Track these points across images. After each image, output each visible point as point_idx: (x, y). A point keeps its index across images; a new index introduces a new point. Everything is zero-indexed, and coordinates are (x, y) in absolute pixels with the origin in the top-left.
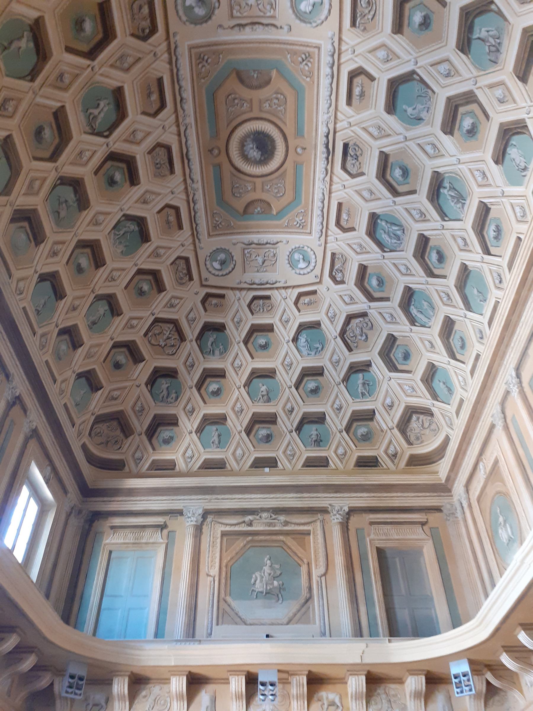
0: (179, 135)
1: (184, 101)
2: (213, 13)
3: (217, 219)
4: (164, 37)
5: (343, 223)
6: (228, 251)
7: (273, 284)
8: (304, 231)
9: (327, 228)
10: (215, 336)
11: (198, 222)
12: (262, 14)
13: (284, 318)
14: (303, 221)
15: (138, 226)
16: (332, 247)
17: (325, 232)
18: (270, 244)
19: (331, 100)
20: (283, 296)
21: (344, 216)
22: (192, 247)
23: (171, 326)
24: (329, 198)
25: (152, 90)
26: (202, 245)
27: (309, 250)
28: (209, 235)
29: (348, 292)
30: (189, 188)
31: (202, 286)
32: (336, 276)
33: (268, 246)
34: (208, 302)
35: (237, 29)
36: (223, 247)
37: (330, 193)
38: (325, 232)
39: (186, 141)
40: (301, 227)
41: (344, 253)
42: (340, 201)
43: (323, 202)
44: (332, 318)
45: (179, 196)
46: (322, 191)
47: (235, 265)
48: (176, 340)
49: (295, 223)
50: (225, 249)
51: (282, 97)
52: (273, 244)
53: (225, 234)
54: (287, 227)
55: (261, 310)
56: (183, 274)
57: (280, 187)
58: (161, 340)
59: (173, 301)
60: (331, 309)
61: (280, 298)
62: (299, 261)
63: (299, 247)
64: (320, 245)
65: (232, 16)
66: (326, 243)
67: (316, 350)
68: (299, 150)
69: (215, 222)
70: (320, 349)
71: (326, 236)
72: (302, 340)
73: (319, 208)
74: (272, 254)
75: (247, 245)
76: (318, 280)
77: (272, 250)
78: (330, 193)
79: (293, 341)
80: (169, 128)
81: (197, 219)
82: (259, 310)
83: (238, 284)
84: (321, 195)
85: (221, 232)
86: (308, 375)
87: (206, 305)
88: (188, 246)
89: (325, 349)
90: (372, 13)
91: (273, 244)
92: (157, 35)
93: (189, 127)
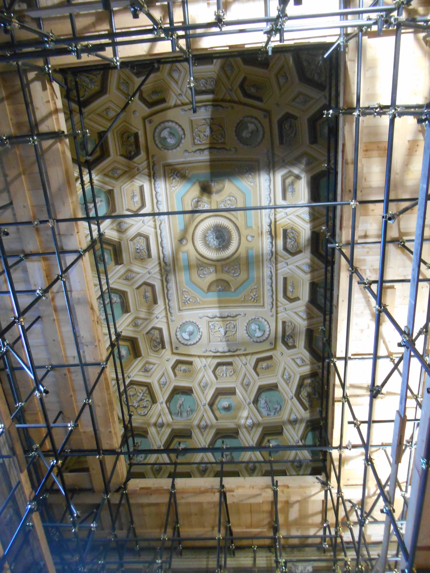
0: (155, 228)
1: (160, 203)
2: (180, 142)
3: (186, 296)
4: (145, 158)
5: (289, 295)
6: (196, 324)
7: (234, 352)
8: (258, 304)
9: (277, 300)
10: (183, 399)
11: (170, 298)
12: (216, 141)
13: (245, 381)
14: (257, 296)
15: (120, 299)
16: (282, 316)
17: (275, 304)
18: (230, 317)
19: (270, 197)
20: (244, 362)
21: (290, 288)
22: (165, 320)
23: (145, 389)
24: (276, 274)
25: (135, 193)
26: (173, 318)
27: (263, 320)
28: (180, 310)
29: (300, 355)
30: (163, 270)
31: (173, 353)
32: (288, 342)
33: (229, 318)
34: (177, 368)
35: (198, 152)
36: (191, 320)
37: (276, 270)
38: (275, 304)
39: (161, 233)
40: (255, 301)
41: (293, 321)
42: (285, 276)
43: (271, 279)
44: (288, 380)
45: (154, 276)
46: (269, 269)
47: (201, 336)
48: (148, 402)
49: (250, 298)
50: (193, 322)
51: (234, 199)
52: (233, 317)
53: (192, 309)
54: (244, 301)
55: (225, 375)
56: (157, 342)
57: (236, 268)
58: (135, 402)
59: (147, 366)
60: (286, 372)
61: (241, 364)
62: (255, 331)
63: (255, 319)
64: (272, 316)
65: (194, 144)
66: (277, 313)
67: (274, 411)
68: (249, 238)
69: (184, 299)
70: (278, 409)
71: (277, 307)
72: (262, 402)
73: (268, 283)
74: (232, 326)
75: (212, 318)
76: (273, 347)
77: (232, 322)
78: (276, 270)
79: (254, 403)
80: (147, 223)
81: (169, 296)
82: (223, 375)
83: (204, 352)
84: (269, 273)
85: (189, 308)
86: (269, 434)
87: (176, 371)
88: (162, 318)
89: (283, 408)
90: (294, 132)
91: (233, 317)
92: (140, 156)
93: (163, 222)
